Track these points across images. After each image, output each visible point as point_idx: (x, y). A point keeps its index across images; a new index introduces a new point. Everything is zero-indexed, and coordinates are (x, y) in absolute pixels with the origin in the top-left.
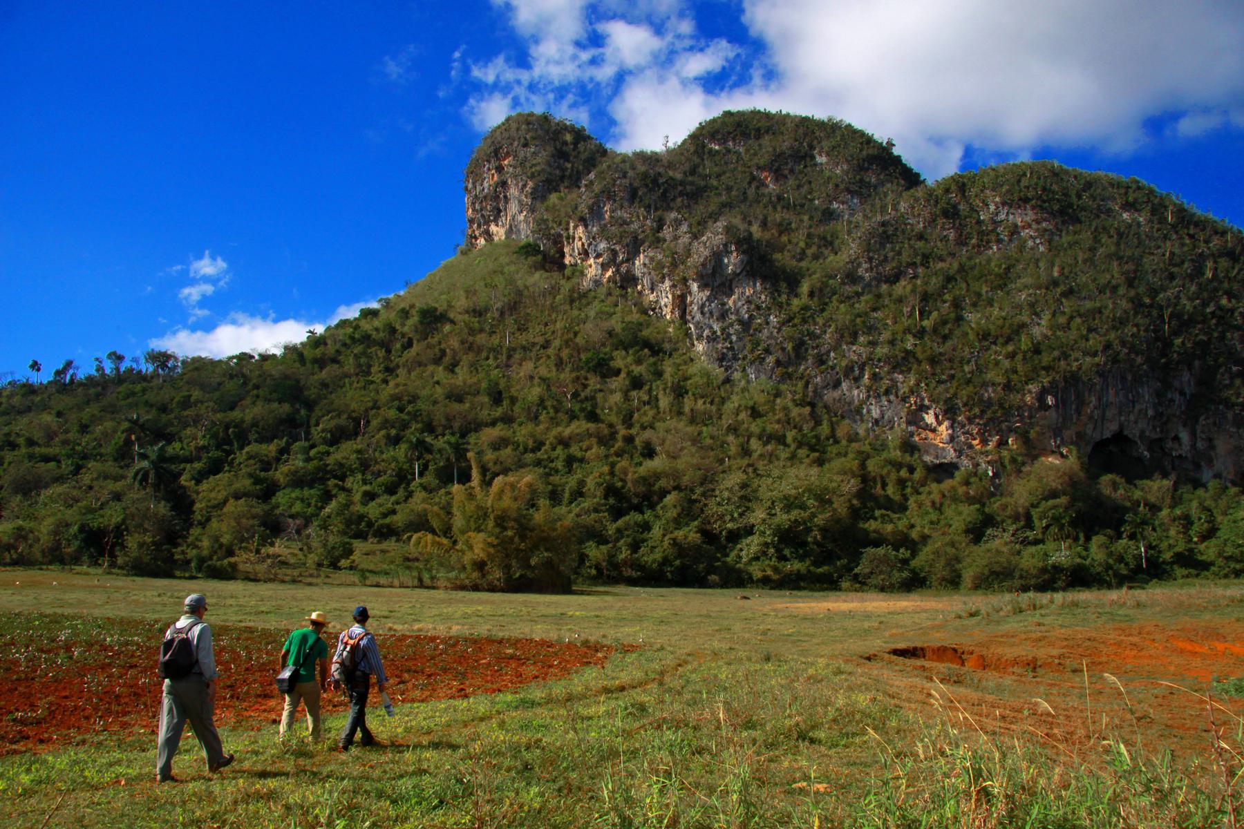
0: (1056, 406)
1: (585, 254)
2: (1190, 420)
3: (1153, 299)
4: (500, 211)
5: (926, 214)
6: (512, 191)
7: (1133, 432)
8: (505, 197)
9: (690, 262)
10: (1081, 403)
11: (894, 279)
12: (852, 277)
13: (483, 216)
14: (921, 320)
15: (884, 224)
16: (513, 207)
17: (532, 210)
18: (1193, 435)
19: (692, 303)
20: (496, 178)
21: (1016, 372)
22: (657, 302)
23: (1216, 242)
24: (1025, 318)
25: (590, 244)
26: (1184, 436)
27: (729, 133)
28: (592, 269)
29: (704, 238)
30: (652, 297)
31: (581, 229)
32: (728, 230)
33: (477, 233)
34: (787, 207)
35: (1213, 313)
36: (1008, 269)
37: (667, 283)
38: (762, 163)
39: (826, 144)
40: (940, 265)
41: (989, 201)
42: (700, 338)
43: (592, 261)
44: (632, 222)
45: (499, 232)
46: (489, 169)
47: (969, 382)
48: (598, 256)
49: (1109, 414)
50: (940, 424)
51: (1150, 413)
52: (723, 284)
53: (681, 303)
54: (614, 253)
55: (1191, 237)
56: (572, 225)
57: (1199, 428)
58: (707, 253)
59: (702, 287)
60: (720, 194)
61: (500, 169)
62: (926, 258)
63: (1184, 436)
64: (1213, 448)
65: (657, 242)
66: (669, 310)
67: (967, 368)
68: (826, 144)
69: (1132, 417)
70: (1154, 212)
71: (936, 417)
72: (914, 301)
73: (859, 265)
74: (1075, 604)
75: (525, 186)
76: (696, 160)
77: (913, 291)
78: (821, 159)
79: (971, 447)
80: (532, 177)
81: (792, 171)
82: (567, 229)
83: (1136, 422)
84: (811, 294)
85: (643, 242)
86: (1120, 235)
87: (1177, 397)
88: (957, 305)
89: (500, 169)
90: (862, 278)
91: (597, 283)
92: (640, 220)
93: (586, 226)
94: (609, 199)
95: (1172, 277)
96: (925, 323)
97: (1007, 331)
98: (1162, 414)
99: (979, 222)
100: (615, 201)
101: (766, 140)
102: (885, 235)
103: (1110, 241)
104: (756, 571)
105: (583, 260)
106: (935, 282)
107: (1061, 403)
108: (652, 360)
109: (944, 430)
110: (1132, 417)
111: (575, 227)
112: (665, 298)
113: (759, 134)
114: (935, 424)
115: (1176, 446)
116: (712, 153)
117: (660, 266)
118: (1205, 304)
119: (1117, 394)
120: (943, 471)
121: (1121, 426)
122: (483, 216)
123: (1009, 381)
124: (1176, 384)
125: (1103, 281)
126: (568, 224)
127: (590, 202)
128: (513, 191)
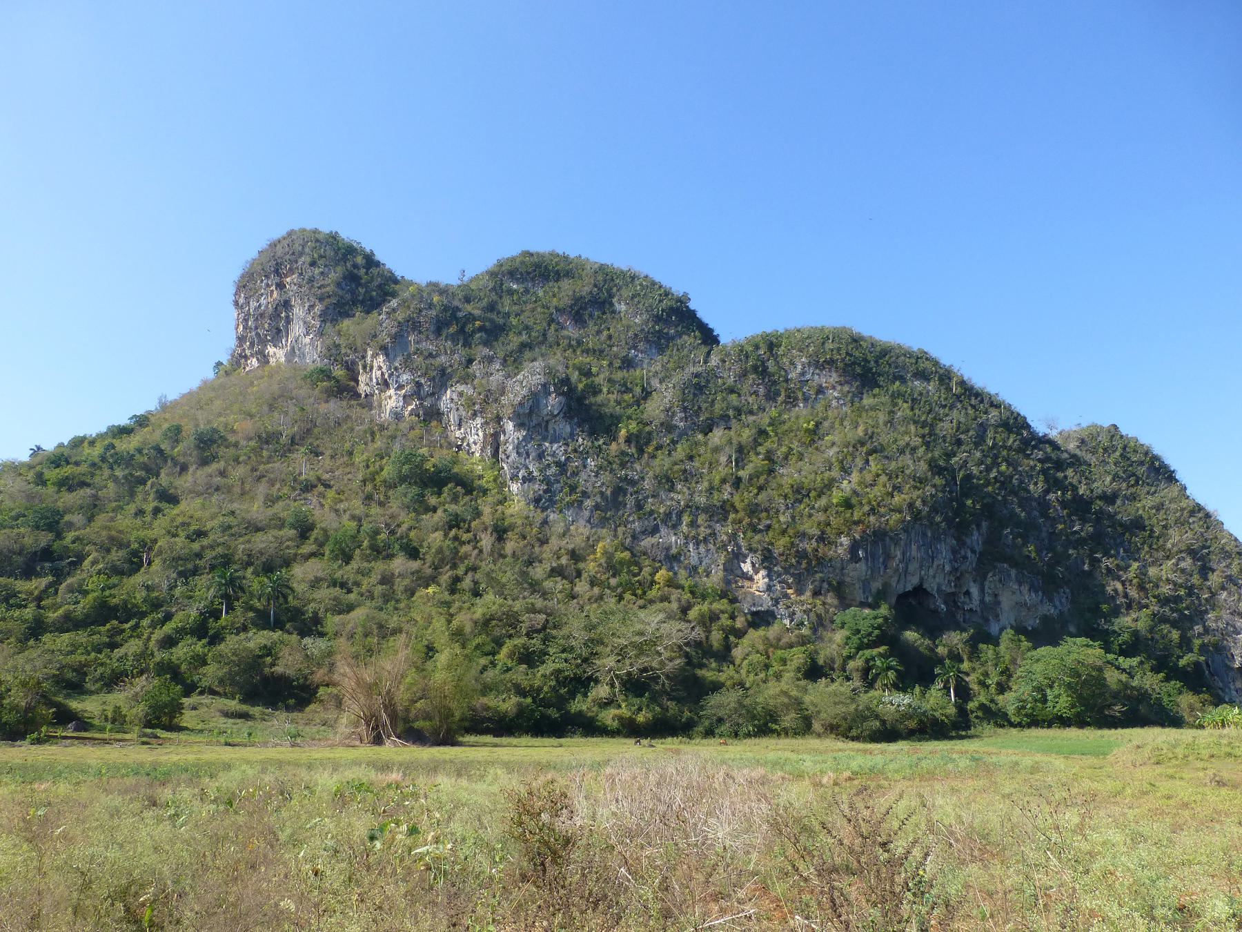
0: (866, 558)
1: (385, 384)
2: (981, 578)
3: (947, 461)
4: (279, 331)
5: (737, 368)
6: (296, 310)
7: (931, 586)
8: (287, 317)
9: (504, 400)
10: (888, 557)
11: (707, 429)
12: (668, 427)
13: (258, 335)
14: (737, 471)
15: (697, 375)
16: (297, 329)
17: (321, 334)
18: (982, 590)
19: (506, 442)
20: (275, 295)
21: (829, 524)
22: (463, 440)
23: (994, 413)
24: (835, 473)
25: (391, 375)
26: (975, 591)
27: (529, 273)
28: (392, 401)
29: (520, 377)
30: (458, 434)
31: (381, 358)
32: (549, 372)
33: (248, 352)
34: (587, 351)
35: (995, 478)
36: (817, 425)
37: (479, 421)
38: (561, 306)
39: (626, 293)
40: (751, 418)
41: (796, 360)
42: (514, 478)
43: (392, 392)
44: (437, 355)
45: (277, 354)
46: (268, 285)
47: (784, 532)
48: (400, 387)
49: (911, 568)
50: (757, 573)
51: (947, 568)
52: (539, 425)
53: (494, 443)
54: (419, 385)
55: (973, 407)
56: (370, 353)
57: (987, 584)
58: (524, 392)
59: (519, 426)
60: (520, 333)
61: (281, 286)
62: (739, 411)
63: (975, 591)
64: (998, 603)
65: (467, 379)
66: (478, 447)
67: (782, 519)
68: (626, 293)
69: (931, 572)
70: (941, 380)
71: (753, 565)
72: (731, 451)
73: (674, 414)
74: (160, 776)
75: (312, 307)
76: (494, 297)
77: (730, 442)
78: (621, 307)
79: (787, 596)
80: (321, 299)
81: (591, 316)
82: (364, 357)
83: (934, 577)
84: (628, 441)
85: (450, 378)
86: (913, 400)
87: (969, 554)
88: (769, 456)
89: (281, 286)
90: (676, 426)
91: (398, 416)
92: (449, 355)
93: (387, 355)
94: (414, 329)
95: (959, 443)
96: (741, 473)
97: (819, 484)
98: (957, 570)
99: (787, 381)
100: (420, 332)
101: (566, 284)
102: (698, 387)
103: (905, 405)
104: (608, 717)
105: (381, 391)
106: (746, 435)
107: (871, 556)
108: (467, 498)
109: (761, 579)
110: (931, 572)
111: (375, 356)
112: (474, 435)
113: (558, 276)
114: (751, 572)
115: (967, 600)
116: (511, 292)
117: (471, 403)
118: (988, 469)
119: (919, 549)
120: (761, 619)
121: (922, 579)
122: (258, 335)
123: (823, 532)
124: (968, 541)
125: (902, 443)
126: (365, 351)
127: (394, 331)
128: (298, 312)
